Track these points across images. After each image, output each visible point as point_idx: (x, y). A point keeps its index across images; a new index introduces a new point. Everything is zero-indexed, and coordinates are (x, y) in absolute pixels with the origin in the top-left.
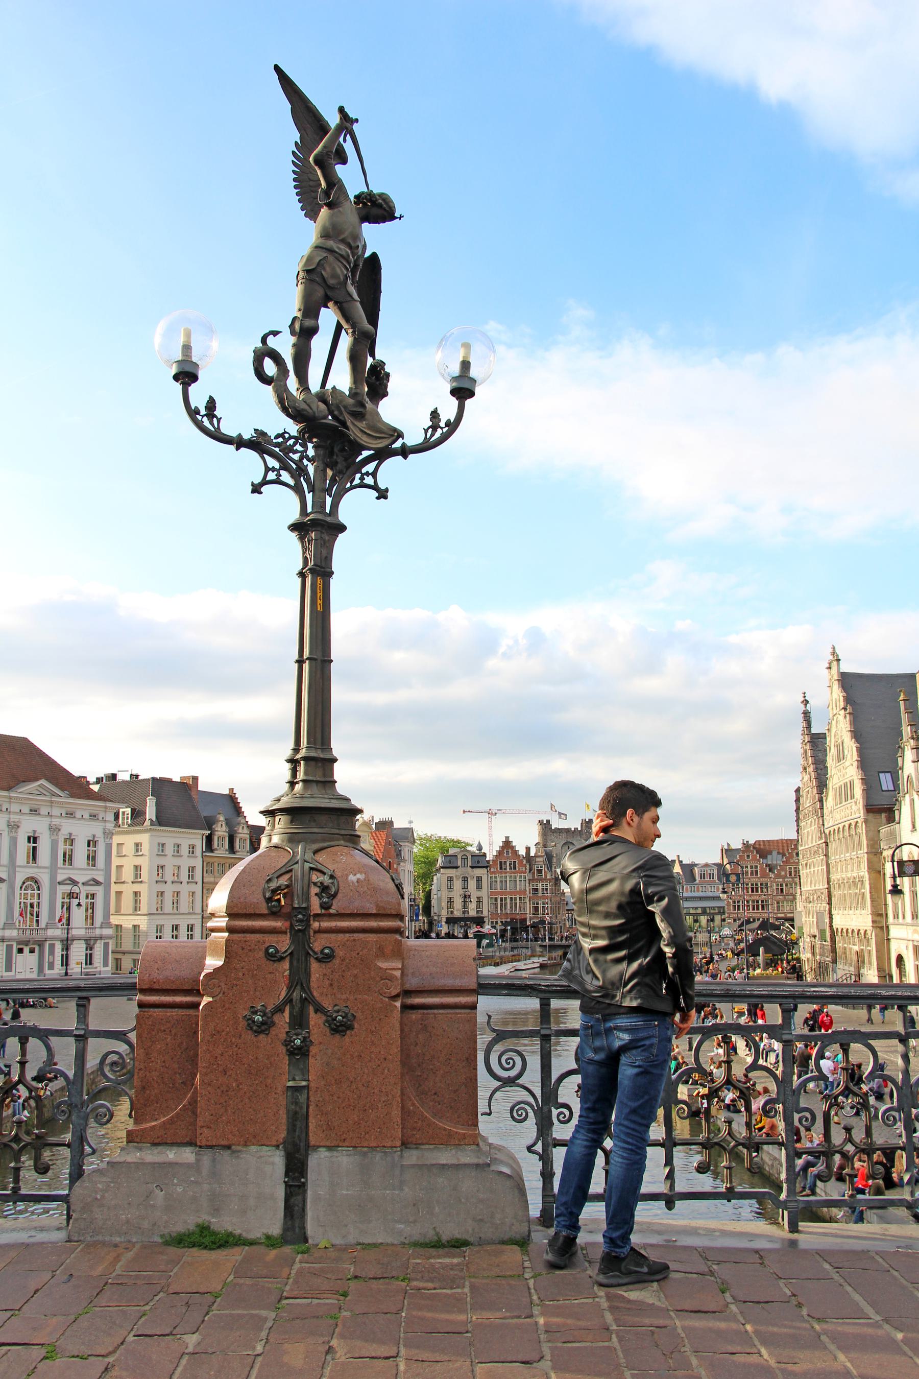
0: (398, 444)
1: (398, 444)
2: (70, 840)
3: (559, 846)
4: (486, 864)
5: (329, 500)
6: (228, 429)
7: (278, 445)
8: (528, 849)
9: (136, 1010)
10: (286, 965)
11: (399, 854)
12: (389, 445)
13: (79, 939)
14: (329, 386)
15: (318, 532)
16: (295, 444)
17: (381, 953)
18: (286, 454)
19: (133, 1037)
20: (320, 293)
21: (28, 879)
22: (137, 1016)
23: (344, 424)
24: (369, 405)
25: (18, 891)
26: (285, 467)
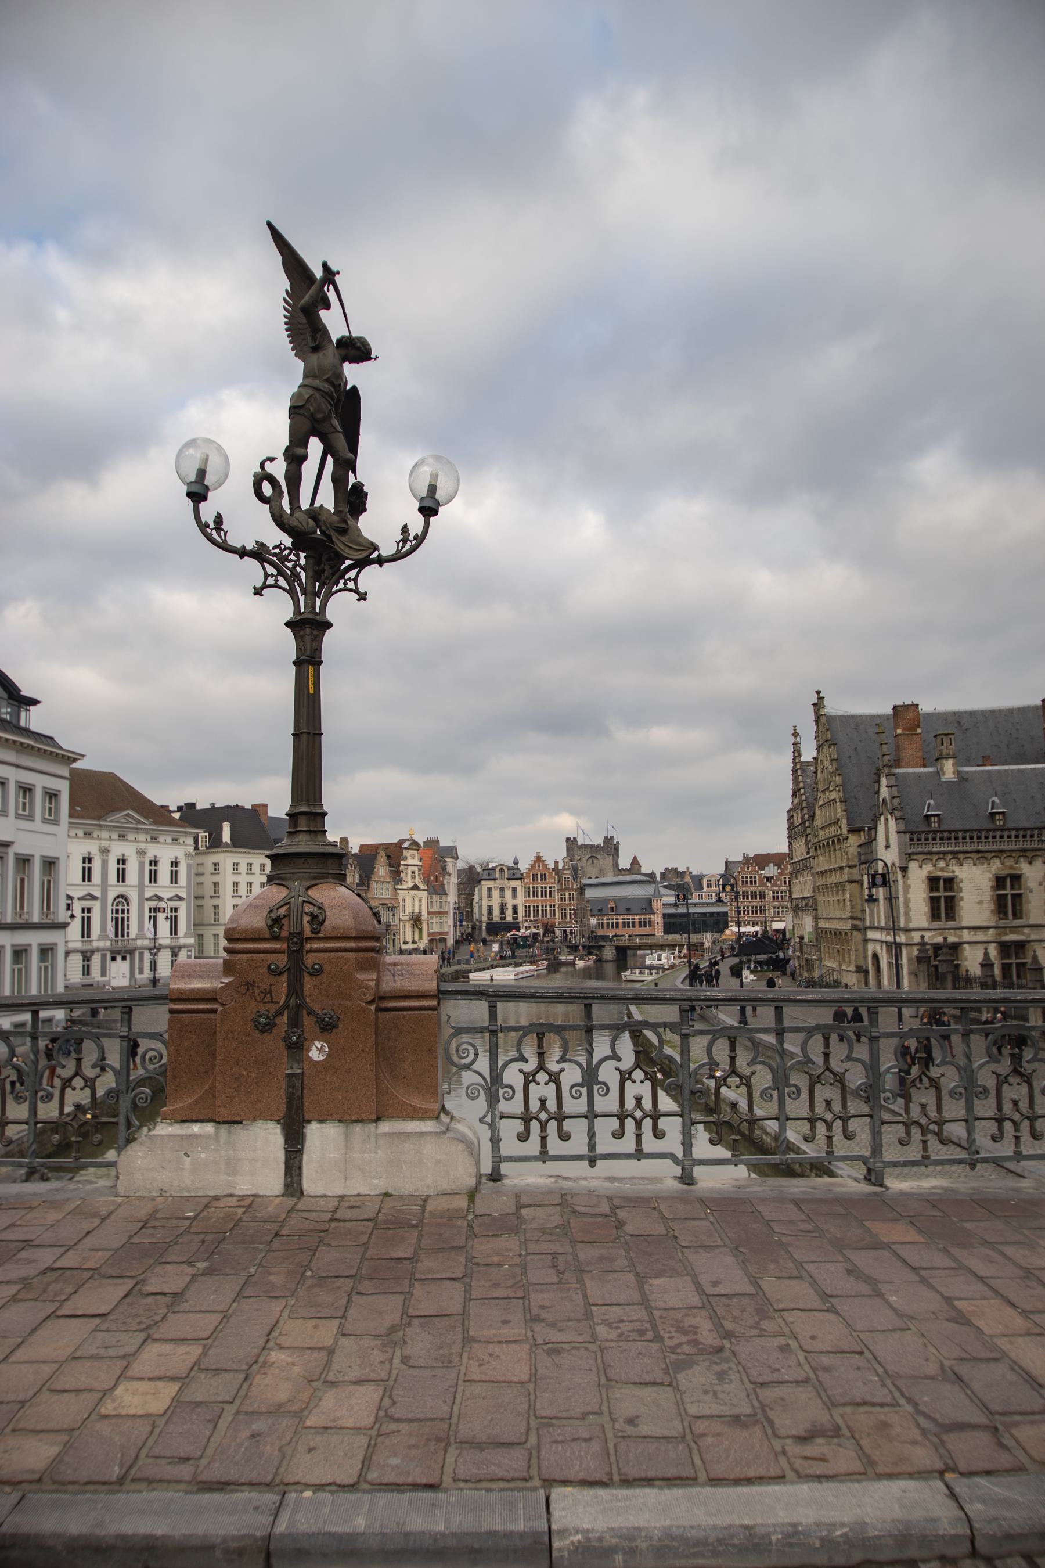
0: (375, 555)
1: (375, 555)
2: (154, 863)
3: (584, 860)
4: (519, 876)
5: (318, 602)
6: (234, 541)
7: (275, 555)
8: (557, 863)
9: (168, 1015)
10: (284, 978)
11: (444, 868)
12: (368, 556)
13: (166, 947)
14: (317, 504)
15: (309, 629)
16: (290, 554)
17: (363, 967)
18: (283, 563)
19: (166, 1036)
20: (307, 425)
21: (118, 897)
22: (169, 1021)
23: (329, 537)
24: (351, 522)
25: (110, 908)
26: (281, 573)
